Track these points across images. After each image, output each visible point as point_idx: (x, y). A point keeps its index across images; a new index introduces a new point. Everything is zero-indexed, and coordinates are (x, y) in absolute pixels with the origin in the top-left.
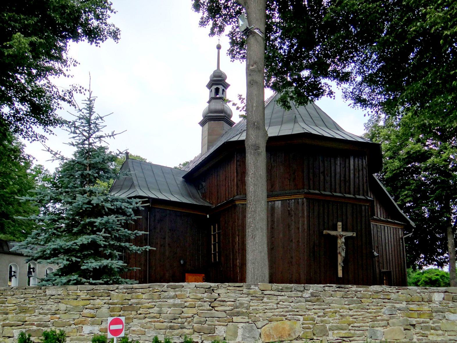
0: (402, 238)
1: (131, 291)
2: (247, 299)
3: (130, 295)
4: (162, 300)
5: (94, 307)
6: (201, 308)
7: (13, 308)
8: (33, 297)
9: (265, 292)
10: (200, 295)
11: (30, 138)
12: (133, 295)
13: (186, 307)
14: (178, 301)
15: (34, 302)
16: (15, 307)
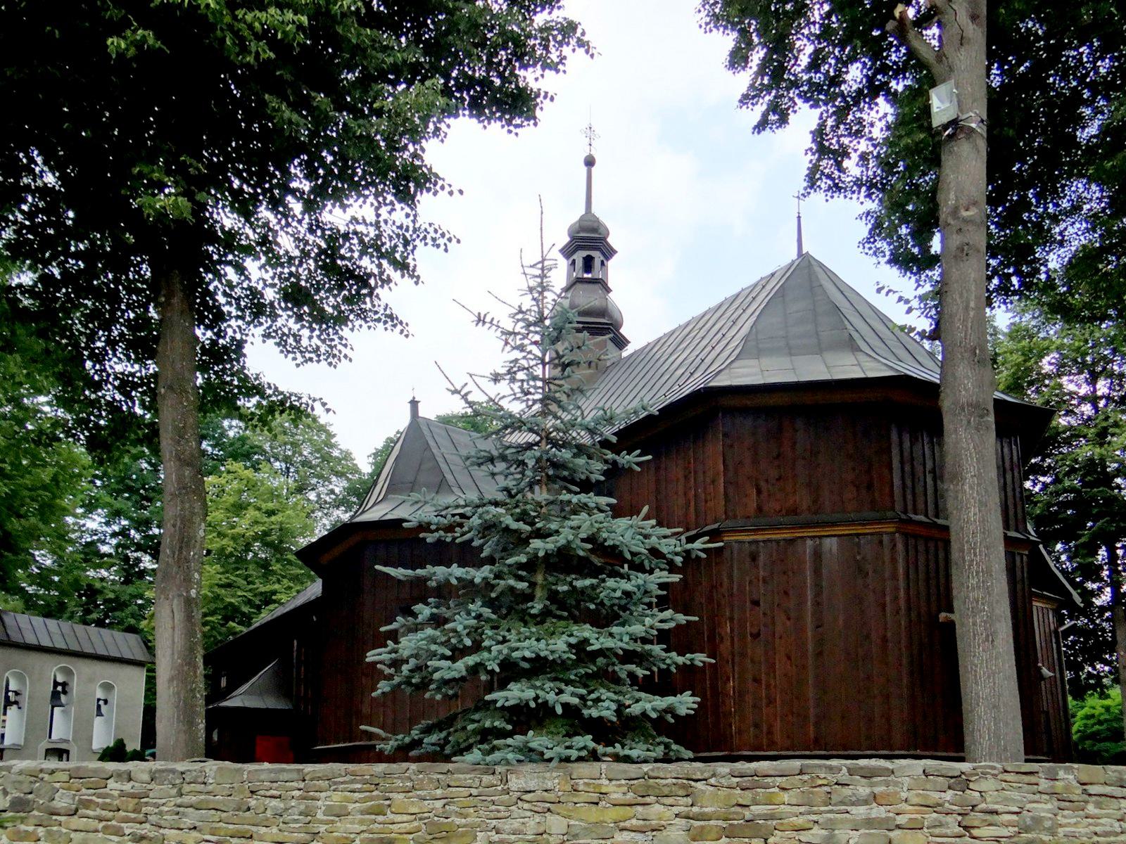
0: (1056, 631)
1: (752, 783)
2: (1049, 806)
3: (748, 794)
4: (835, 808)
5: (645, 826)
6: (937, 831)
7: (408, 827)
8: (471, 795)
9: (1093, 789)
10: (935, 796)
11: (298, 355)
12: (758, 794)
13: (898, 827)
14: (878, 812)
15: (472, 810)
16: (416, 824)
